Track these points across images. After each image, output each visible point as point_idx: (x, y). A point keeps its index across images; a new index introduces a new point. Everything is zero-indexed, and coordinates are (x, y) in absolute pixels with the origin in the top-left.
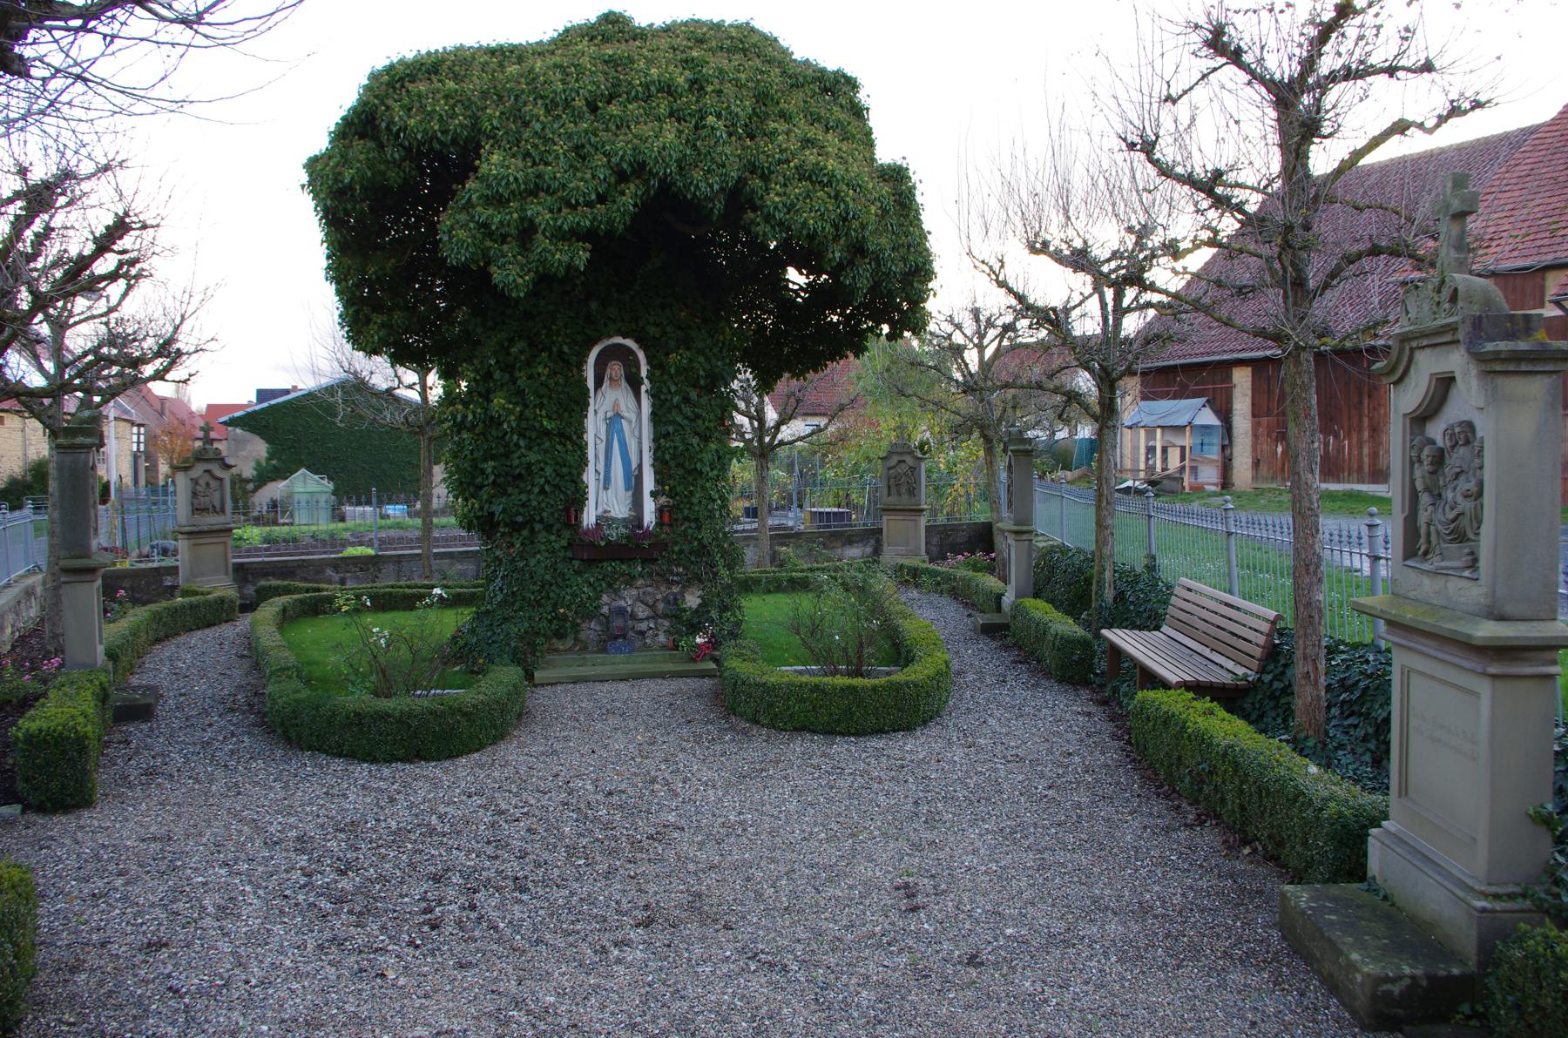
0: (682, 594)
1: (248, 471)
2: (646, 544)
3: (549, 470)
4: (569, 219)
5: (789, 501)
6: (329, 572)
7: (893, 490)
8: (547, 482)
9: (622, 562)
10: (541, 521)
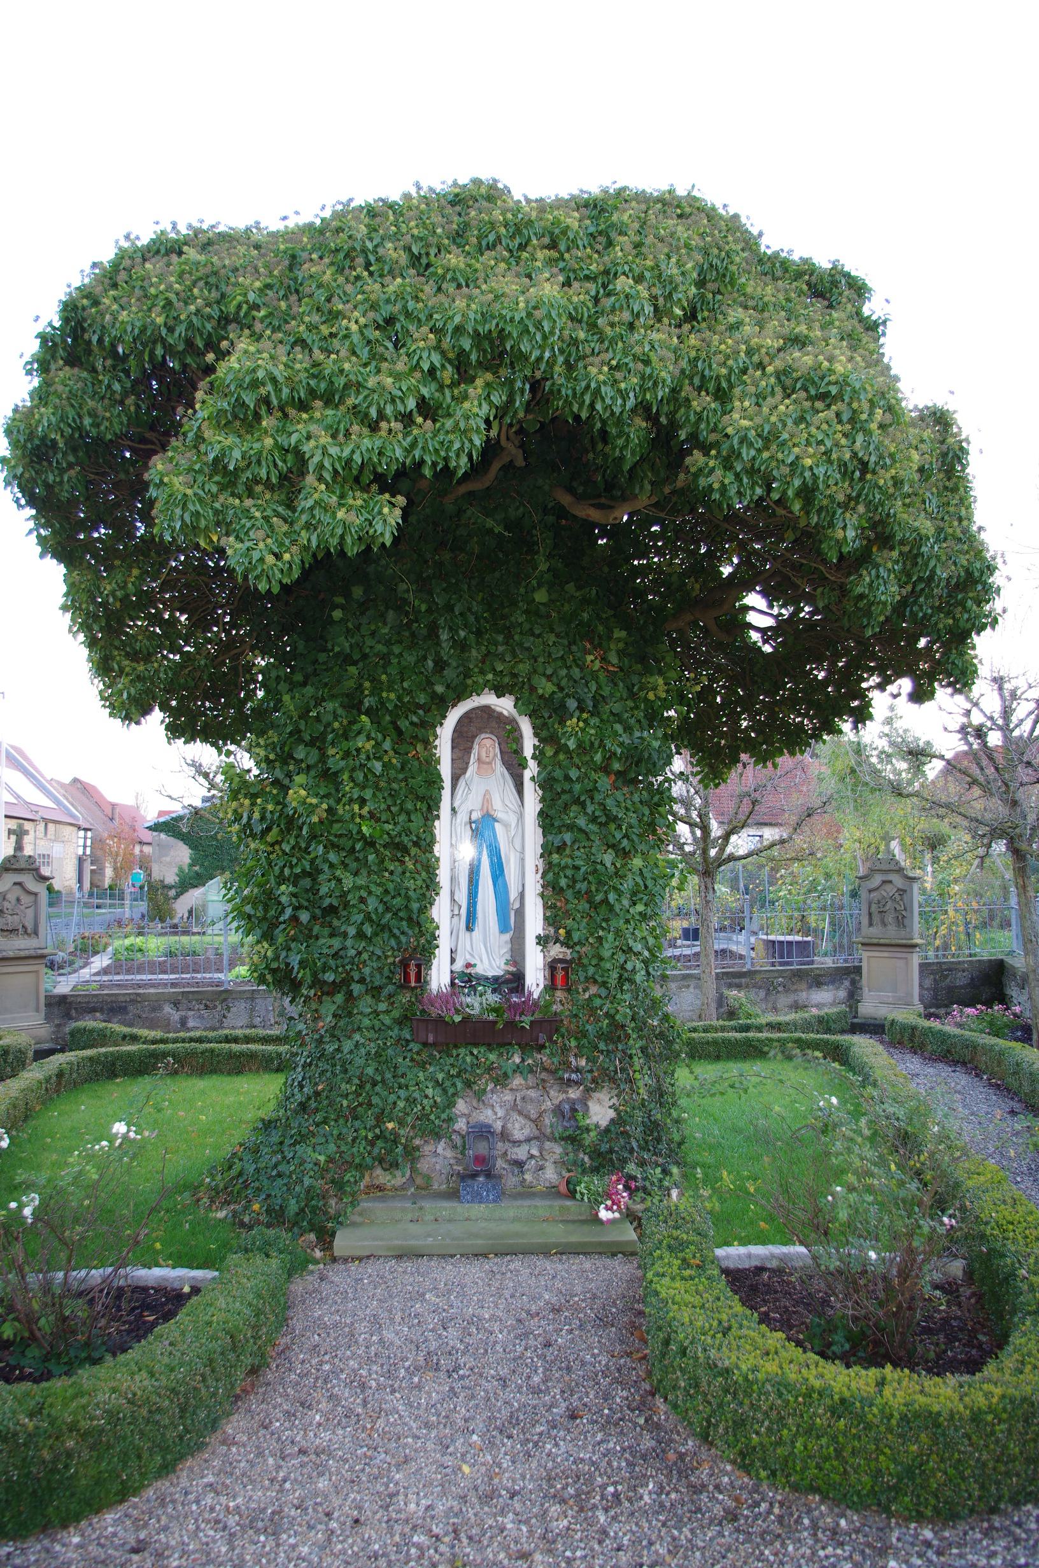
0: (584, 1101)
1: (171, 878)
2: (526, 1021)
3: (372, 904)
4: (363, 445)
5: (737, 924)
6: (167, 1009)
7: (876, 918)
8: (368, 918)
9: (490, 1047)
10: (362, 981)
